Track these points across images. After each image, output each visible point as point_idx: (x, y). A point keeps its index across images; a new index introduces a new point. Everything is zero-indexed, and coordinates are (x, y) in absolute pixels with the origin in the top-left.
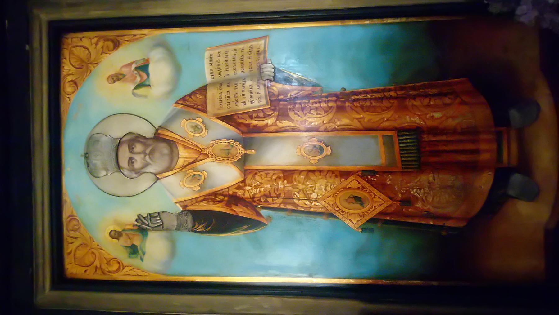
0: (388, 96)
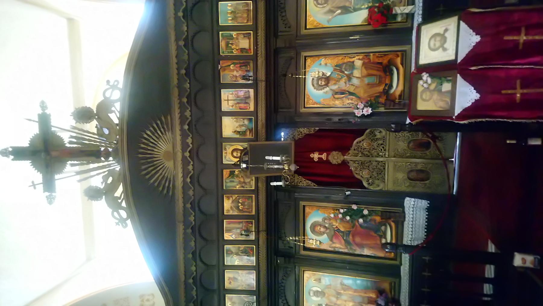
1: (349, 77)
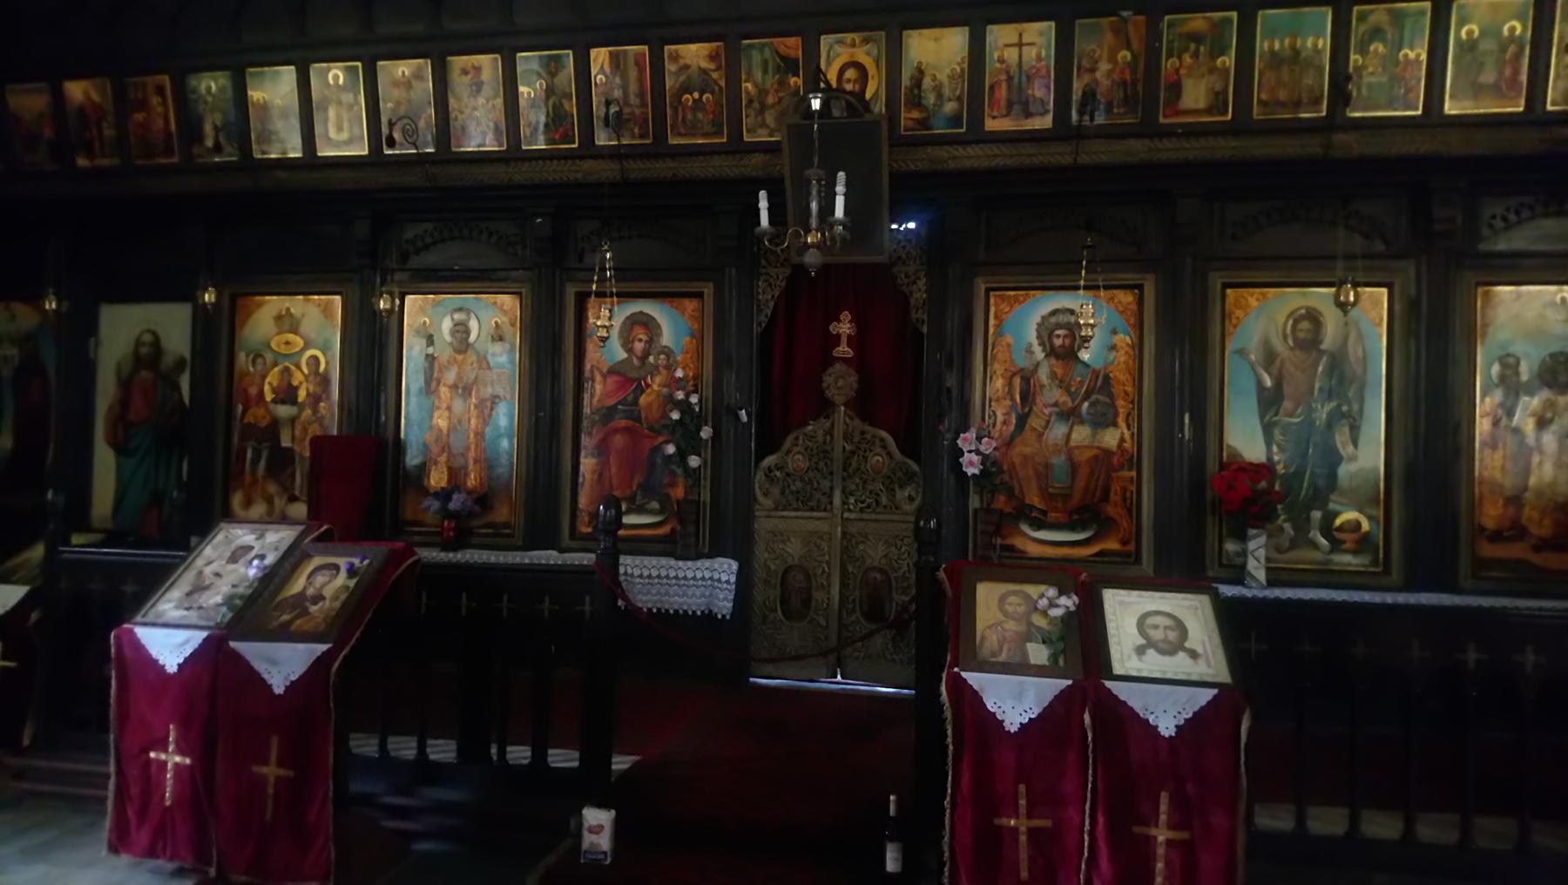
0: (1498, 475)
1: (1070, 415)
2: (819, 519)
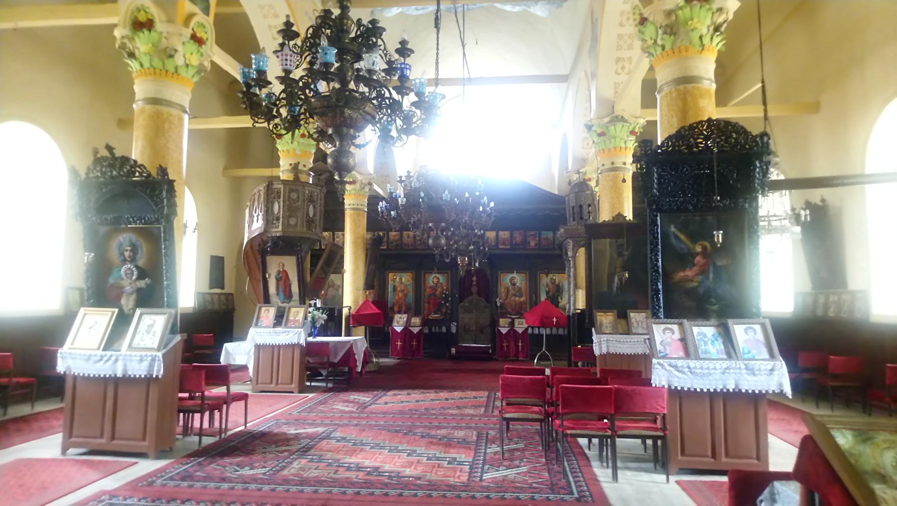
1: (515, 295)
2: (776, 220)
